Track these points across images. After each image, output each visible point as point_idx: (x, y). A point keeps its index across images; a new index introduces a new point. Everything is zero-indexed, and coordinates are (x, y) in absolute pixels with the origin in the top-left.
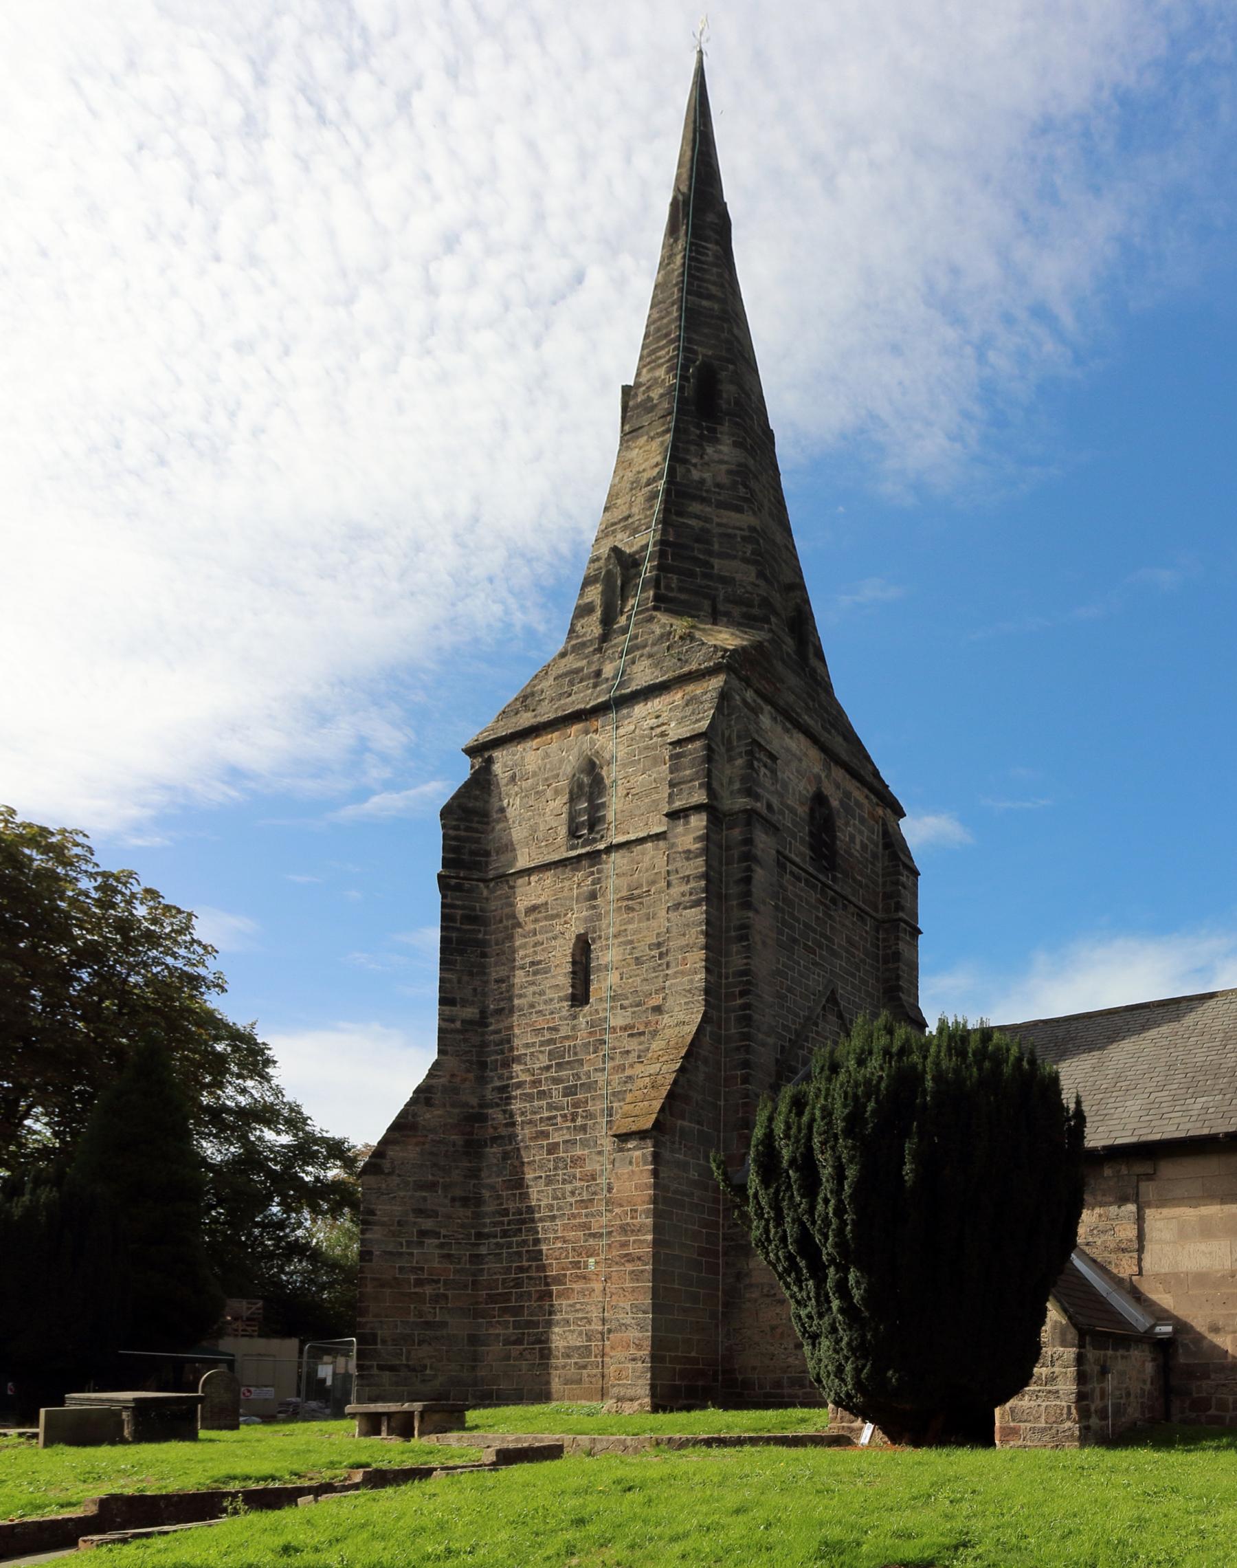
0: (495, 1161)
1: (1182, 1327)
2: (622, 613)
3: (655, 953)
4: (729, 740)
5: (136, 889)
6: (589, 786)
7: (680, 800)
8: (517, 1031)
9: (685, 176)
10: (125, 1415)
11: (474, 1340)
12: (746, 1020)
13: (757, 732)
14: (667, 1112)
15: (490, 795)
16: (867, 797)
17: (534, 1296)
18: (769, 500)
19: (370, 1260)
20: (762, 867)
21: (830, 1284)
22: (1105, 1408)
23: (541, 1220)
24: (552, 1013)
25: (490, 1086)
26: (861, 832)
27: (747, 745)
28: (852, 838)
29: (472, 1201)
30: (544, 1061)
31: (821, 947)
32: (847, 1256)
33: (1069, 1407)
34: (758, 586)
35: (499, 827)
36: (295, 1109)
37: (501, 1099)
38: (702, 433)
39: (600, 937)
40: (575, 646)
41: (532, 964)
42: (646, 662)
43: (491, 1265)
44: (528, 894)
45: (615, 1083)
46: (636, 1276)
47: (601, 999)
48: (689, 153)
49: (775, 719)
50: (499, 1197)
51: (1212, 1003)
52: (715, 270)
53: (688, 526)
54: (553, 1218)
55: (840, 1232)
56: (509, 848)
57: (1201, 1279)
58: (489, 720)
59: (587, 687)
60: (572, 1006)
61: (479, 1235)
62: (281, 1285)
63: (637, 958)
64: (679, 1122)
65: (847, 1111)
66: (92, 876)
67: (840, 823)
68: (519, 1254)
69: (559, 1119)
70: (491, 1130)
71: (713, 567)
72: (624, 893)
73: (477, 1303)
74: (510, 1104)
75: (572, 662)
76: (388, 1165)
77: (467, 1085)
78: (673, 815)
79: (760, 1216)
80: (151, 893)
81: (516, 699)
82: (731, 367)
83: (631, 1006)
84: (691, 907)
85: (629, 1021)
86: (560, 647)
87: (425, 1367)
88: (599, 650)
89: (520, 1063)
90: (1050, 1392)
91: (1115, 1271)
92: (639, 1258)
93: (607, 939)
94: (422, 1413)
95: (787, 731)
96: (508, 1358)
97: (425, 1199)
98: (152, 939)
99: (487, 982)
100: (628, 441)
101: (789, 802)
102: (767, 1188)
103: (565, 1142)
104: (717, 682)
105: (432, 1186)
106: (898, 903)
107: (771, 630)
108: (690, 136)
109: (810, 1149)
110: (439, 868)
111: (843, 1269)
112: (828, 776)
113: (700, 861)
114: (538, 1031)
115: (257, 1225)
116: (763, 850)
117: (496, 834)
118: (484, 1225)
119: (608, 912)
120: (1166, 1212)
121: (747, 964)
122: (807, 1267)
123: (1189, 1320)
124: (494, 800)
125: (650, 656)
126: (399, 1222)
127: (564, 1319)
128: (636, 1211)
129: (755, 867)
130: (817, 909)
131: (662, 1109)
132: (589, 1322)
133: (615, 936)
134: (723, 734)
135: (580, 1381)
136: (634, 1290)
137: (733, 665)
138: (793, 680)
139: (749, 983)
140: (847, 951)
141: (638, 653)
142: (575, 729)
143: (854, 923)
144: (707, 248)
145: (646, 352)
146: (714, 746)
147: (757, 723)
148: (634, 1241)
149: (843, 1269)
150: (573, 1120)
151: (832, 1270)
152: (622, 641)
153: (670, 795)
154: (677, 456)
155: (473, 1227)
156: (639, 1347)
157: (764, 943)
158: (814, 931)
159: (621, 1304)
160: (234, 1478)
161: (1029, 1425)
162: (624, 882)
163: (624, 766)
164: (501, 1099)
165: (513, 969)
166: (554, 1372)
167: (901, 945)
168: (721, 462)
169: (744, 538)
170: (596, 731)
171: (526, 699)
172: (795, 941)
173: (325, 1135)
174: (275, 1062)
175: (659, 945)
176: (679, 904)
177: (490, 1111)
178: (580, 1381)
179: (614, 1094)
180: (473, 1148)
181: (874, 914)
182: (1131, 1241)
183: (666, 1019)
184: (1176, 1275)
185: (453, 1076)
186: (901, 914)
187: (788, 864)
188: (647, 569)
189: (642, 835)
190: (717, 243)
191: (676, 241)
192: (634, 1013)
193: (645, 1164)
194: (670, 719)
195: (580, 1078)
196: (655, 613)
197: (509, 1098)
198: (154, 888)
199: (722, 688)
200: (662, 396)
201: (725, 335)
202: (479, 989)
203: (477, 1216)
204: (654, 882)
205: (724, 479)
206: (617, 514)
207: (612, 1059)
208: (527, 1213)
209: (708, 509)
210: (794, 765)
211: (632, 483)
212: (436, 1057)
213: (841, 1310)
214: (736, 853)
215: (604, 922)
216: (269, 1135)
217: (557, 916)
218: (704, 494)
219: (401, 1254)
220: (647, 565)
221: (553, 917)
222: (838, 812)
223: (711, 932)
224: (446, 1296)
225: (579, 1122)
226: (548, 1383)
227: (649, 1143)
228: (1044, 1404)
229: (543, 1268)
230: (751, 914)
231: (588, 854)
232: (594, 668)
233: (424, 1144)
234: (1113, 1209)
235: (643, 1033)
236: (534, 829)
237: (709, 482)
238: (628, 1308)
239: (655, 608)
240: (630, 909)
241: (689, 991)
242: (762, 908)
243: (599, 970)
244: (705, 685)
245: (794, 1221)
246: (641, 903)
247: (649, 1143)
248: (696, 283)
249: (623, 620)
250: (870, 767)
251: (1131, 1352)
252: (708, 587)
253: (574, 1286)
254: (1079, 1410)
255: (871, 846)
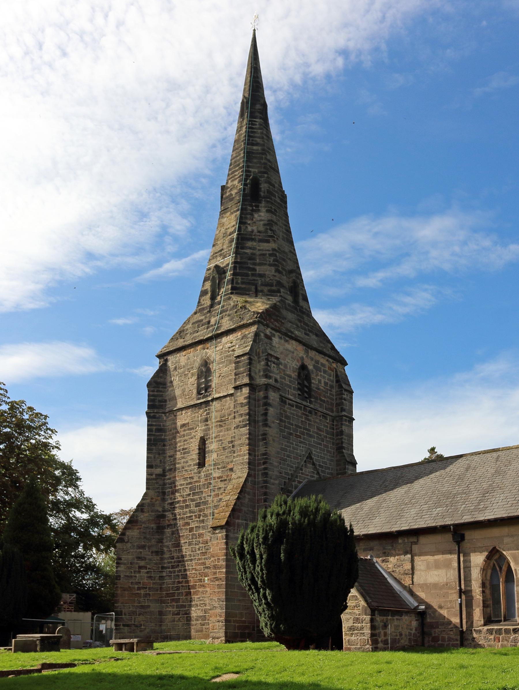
0: (169, 535)
1: (429, 606)
2: (218, 295)
3: (231, 445)
4: (259, 354)
5: (25, 407)
6: (205, 371)
7: (239, 381)
8: (177, 479)
9: (247, 89)
10: (38, 642)
11: (161, 613)
12: (266, 475)
13: (271, 349)
14: (232, 517)
15: (166, 375)
16: (327, 360)
17: (184, 594)
18: (283, 232)
19: (120, 580)
20: (272, 407)
21: (261, 595)
22: (387, 640)
23: (187, 561)
24: (191, 471)
25: (166, 502)
26: (324, 377)
27: (266, 356)
28: (320, 381)
29: (159, 553)
30: (188, 491)
31: (303, 434)
32: (266, 584)
33: (368, 639)
34: (275, 276)
35: (170, 389)
36: (89, 500)
37: (171, 508)
38: (253, 209)
39: (209, 438)
40: (200, 310)
41: (183, 449)
42: (227, 318)
43: (167, 580)
44: (182, 419)
45: (215, 502)
46: (219, 586)
47: (210, 465)
48: (249, 79)
49: (281, 338)
50: (170, 551)
51: (460, 460)
52: (259, 131)
53: (246, 253)
54: (191, 560)
55: (262, 577)
56: (174, 398)
57: (435, 586)
58: (166, 342)
59: (204, 329)
60: (199, 468)
61: (163, 568)
62: (83, 586)
63: (224, 447)
64: (237, 521)
65: (263, 536)
66: (7, 403)
67: (313, 376)
68: (178, 576)
69: (194, 517)
70: (167, 522)
71: (256, 270)
72: (219, 419)
73: (162, 597)
74: (175, 510)
75: (199, 317)
76: (127, 539)
77: (157, 502)
78: (236, 388)
79: (240, 570)
80: (31, 409)
81: (177, 333)
82: (266, 175)
83: (221, 468)
84: (243, 427)
85: (220, 475)
86: (194, 310)
87: (141, 625)
88: (209, 312)
89: (178, 493)
90: (361, 633)
91: (403, 583)
92: (220, 579)
93: (212, 439)
94: (137, 643)
95: (287, 341)
96: (174, 621)
97: (141, 552)
98: (30, 428)
99: (165, 457)
100: (222, 214)
101: (288, 373)
102: (241, 561)
103: (196, 527)
104: (254, 329)
105: (143, 547)
106: (342, 408)
107: (281, 296)
108: (250, 70)
109: (253, 548)
110: (146, 409)
111: (265, 589)
112: (307, 356)
113: (246, 407)
114: (185, 479)
115: (72, 556)
116: (273, 400)
117: (168, 393)
118: (165, 563)
119: (212, 427)
120: (422, 558)
121: (266, 450)
122: (255, 589)
123: (431, 603)
124: (168, 378)
125: (229, 315)
126: (131, 563)
127: (196, 604)
128: (219, 559)
129: (268, 408)
130: (302, 417)
131: (230, 516)
132: (205, 605)
133: (215, 438)
134: (256, 351)
135: (202, 631)
136: (219, 592)
137: (263, 319)
138: (290, 316)
139: (266, 458)
140: (317, 434)
141: (224, 314)
142: (199, 347)
143: (320, 420)
144: (255, 121)
145: (230, 172)
146: (252, 357)
147: (271, 344)
148: (219, 572)
149: (265, 589)
150: (199, 518)
151: (261, 590)
152: (218, 308)
153: (235, 379)
154: (242, 222)
155: (160, 564)
156: (220, 616)
157: (273, 440)
158: (300, 428)
159: (214, 598)
160: (76, 660)
161: (354, 647)
162: (218, 414)
163: (219, 364)
164: (171, 508)
165: (176, 451)
166: (192, 627)
167: (344, 428)
168: (261, 220)
169: (270, 255)
170: (208, 348)
171: (181, 333)
172: (291, 434)
173: (102, 513)
174: (80, 479)
175: (232, 442)
176: (239, 426)
177: (167, 513)
178: (202, 631)
179: (215, 506)
180: (160, 529)
181: (331, 414)
182: (409, 570)
183: (234, 476)
184: (426, 584)
185: (152, 499)
186: (344, 413)
187: (287, 400)
188: (229, 275)
189: (225, 394)
190: (261, 118)
191: (243, 120)
192: (222, 471)
193: (223, 540)
194: (236, 344)
195: (201, 499)
196: (231, 296)
197: (174, 508)
198: (32, 406)
199: (256, 331)
200: (236, 193)
201: (263, 161)
202: (162, 460)
203: (162, 559)
204: (230, 415)
205: (262, 228)
206: (218, 248)
207: (214, 491)
208: (181, 558)
209: (255, 244)
210: (290, 356)
211: (224, 234)
212: (145, 491)
213: (265, 604)
214: (261, 403)
215: (211, 431)
216: (78, 514)
217: (193, 429)
218: (253, 237)
219: (131, 576)
220: (229, 273)
221: (191, 429)
222: (312, 371)
223: (251, 437)
224: (149, 594)
225: (201, 518)
226: (190, 632)
227: (224, 530)
228: (359, 638)
229: (187, 582)
230: (267, 429)
231: (205, 402)
232: (207, 320)
233: (140, 529)
234: (402, 556)
235: (225, 480)
236: (184, 391)
237: (256, 231)
238: (216, 600)
239: (232, 293)
240: (221, 426)
241: (242, 463)
242: (272, 425)
243: (209, 452)
244: (249, 330)
245: (249, 573)
246: (225, 423)
247: (224, 530)
248: (251, 139)
249: (219, 298)
250: (330, 345)
251: (403, 617)
252: (254, 280)
253: (200, 590)
254: (372, 640)
255: (329, 383)
